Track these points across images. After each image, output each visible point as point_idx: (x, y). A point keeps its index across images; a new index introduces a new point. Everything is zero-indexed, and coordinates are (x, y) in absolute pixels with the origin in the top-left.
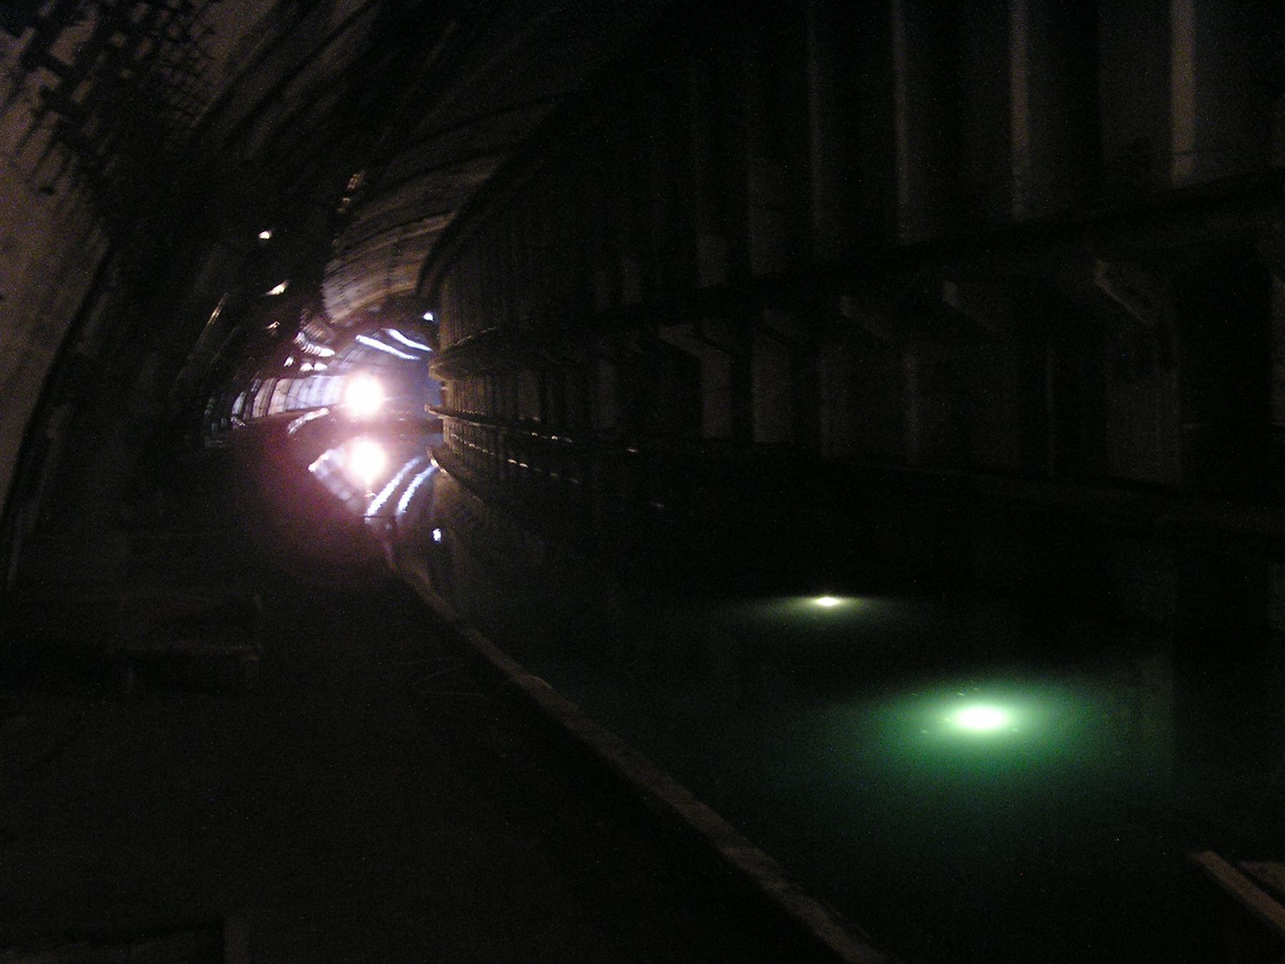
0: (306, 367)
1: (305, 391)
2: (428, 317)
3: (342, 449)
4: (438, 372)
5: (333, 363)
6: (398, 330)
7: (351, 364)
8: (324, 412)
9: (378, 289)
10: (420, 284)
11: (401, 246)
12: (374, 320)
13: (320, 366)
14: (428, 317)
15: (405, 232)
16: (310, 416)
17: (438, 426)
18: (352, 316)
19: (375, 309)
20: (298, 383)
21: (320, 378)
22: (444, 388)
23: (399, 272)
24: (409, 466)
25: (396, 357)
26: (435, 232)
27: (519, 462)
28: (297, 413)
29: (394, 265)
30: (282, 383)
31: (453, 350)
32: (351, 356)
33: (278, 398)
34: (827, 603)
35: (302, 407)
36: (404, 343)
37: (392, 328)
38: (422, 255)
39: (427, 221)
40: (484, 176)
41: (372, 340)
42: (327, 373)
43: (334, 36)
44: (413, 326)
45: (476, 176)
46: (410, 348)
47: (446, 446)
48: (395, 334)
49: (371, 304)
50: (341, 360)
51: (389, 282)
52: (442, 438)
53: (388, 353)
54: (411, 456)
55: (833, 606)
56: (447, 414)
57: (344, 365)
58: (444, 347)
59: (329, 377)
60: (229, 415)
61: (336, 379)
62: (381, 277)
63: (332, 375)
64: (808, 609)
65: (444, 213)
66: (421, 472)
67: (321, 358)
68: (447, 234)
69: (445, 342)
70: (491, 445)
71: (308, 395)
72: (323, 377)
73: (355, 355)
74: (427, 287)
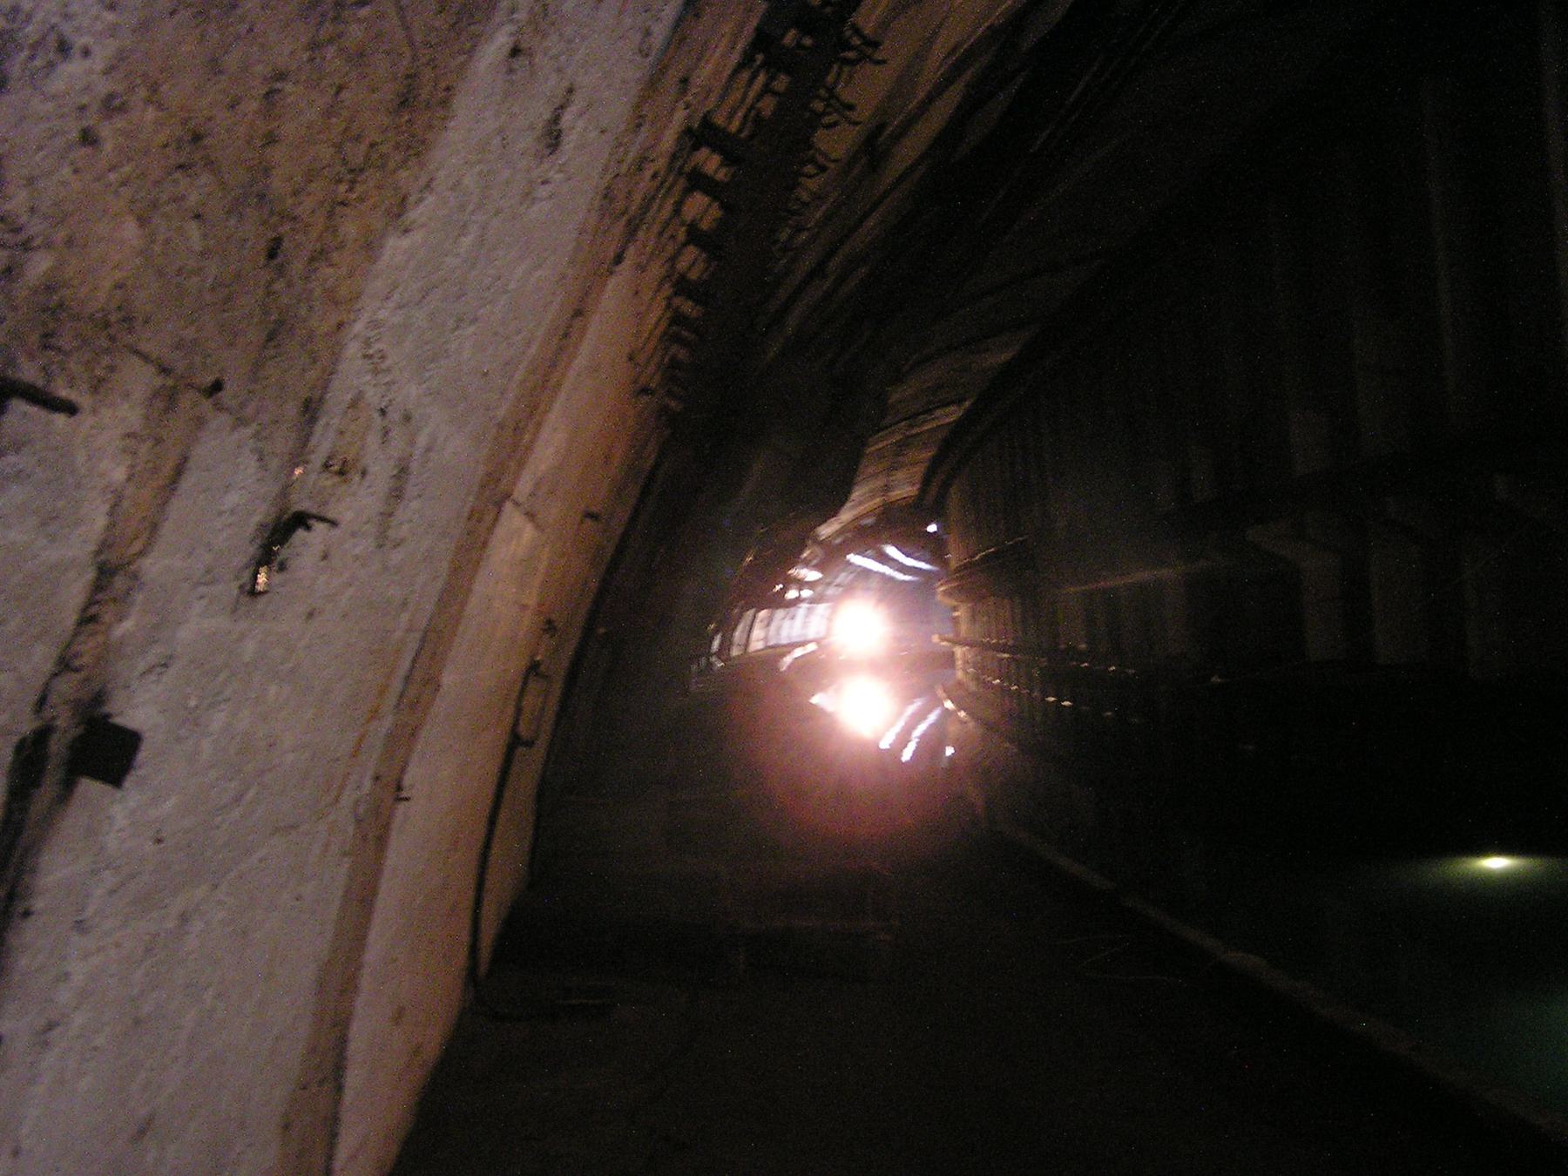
0: (792, 594)
1: (787, 623)
2: (932, 528)
3: (831, 691)
4: (947, 593)
5: (819, 589)
6: (893, 545)
7: (841, 589)
8: (811, 647)
9: (872, 497)
10: (923, 491)
11: (903, 445)
12: (866, 536)
13: (806, 593)
14: (932, 528)
15: (911, 426)
16: (798, 652)
17: (949, 659)
18: (839, 533)
19: (869, 521)
20: (780, 613)
21: (804, 606)
22: (956, 614)
23: (900, 475)
24: (911, 709)
25: (891, 579)
26: (949, 424)
27: (1060, 700)
28: (785, 649)
29: (893, 468)
30: (763, 614)
31: (967, 569)
32: (838, 581)
33: (757, 633)
34: (1496, 863)
35: (784, 642)
36: (901, 561)
37: (887, 543)
38: (928, 454)
39: (938, 413)
40: (1004, 357)
41: (866, 559)
42: (813, 601)
43: (880, 201)
44: (912, 540)
45: (999, 356)
46: (907, 567)
47: (960, 684)
48: (891, 551)
49: (862, 516)
50: (829, 584)
51: (887, 488)
52: (954, 674)
53: (883, 575)
54: (908, 700)
55: (1498, 869)
56: (967, 645)
57: (831, 591)
58: (954, 564)
59: (814, 605)
60: (709, 655)
61: (821, 608)
62: (879, 483)
63: (818, 603)
64: (1473, 873)
65: (960, 401)
66: (36, 784)
67: (808, 583)
68: (959, 429)
69: (954, 558)
70: (1023, 681)
71: (791, 627)
72: (807, 605)
73: (843, 577)
74: (934, 490)
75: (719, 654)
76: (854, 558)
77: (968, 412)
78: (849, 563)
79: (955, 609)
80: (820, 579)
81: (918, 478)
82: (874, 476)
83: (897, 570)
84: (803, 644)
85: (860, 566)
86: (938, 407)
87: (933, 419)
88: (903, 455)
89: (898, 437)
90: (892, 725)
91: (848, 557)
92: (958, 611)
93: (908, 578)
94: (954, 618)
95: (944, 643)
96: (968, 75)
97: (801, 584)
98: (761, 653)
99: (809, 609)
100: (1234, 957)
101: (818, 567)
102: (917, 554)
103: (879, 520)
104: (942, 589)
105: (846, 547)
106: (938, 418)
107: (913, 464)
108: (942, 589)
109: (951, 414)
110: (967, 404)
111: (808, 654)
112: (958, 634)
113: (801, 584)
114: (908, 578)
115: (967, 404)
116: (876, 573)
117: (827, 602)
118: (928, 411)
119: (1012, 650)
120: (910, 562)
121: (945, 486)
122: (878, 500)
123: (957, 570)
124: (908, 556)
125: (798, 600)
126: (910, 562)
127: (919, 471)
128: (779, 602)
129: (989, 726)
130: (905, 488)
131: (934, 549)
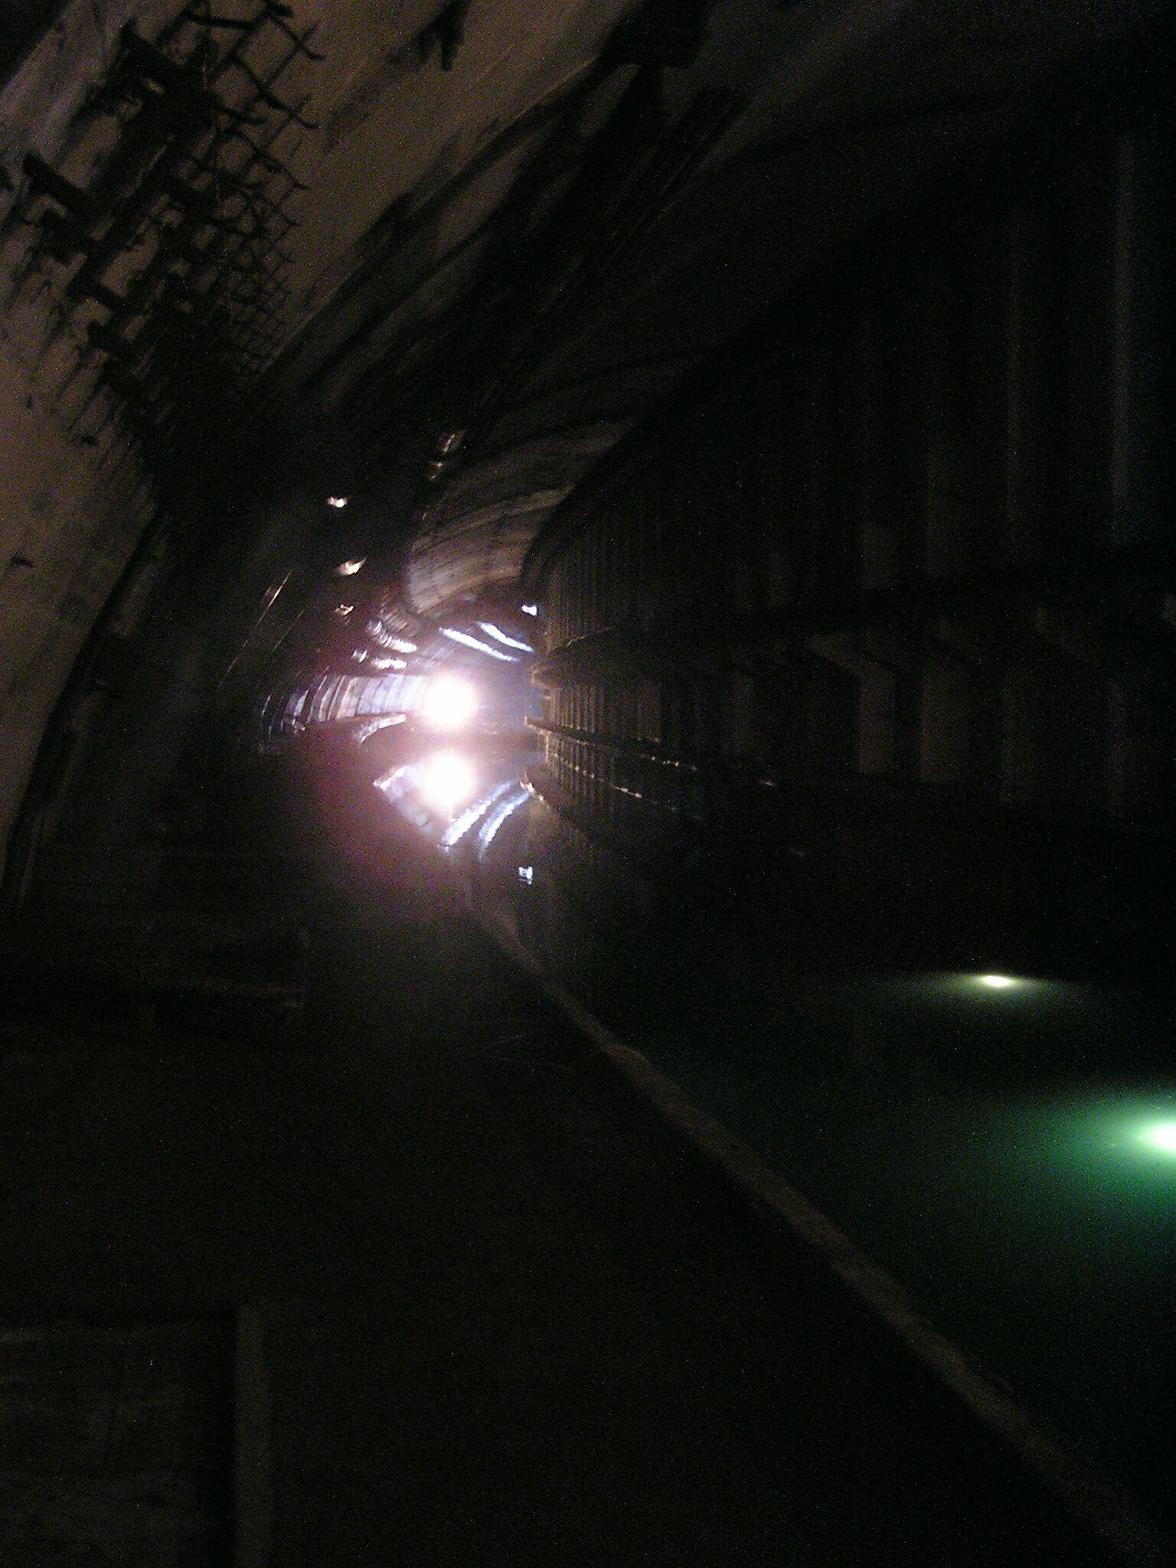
1: (381, 692)
8: (401, 719)
12: (462, 612)
13: (399, 664)
16: (384, 723)
20: (373, 682)
23: (501, 554)
30: (354, 681)
33: (346, 699)
34: (996, 982)
38: (529, 536)
45: (597, 443)
47: (544, 768)
48: (490, 629)
57: (428, 665)
58: (550, 646)
61: (417, 681)
76: (449, 633)
77: (569, 498)
78: (448, 639)
84: (385, 715)
85: (458, 643)
92: (548, 695)
93: (509, 658)
95: (531, 726)
96: (517, 153)
97: (395, 654)
101: (414, 640)
102: (520, 636)
103: (480, 597)
107: (515, 543)
110: (568, 490)
111: (395, 726)
112: (546, 718)
113: (395, 654)
114: (509, 658)
119: (582, 735)
122: (479, 579)
124: (508, 636)
127: (519, 552)
128: (366, 671)
129: (566, 814)
131: (529, 629)
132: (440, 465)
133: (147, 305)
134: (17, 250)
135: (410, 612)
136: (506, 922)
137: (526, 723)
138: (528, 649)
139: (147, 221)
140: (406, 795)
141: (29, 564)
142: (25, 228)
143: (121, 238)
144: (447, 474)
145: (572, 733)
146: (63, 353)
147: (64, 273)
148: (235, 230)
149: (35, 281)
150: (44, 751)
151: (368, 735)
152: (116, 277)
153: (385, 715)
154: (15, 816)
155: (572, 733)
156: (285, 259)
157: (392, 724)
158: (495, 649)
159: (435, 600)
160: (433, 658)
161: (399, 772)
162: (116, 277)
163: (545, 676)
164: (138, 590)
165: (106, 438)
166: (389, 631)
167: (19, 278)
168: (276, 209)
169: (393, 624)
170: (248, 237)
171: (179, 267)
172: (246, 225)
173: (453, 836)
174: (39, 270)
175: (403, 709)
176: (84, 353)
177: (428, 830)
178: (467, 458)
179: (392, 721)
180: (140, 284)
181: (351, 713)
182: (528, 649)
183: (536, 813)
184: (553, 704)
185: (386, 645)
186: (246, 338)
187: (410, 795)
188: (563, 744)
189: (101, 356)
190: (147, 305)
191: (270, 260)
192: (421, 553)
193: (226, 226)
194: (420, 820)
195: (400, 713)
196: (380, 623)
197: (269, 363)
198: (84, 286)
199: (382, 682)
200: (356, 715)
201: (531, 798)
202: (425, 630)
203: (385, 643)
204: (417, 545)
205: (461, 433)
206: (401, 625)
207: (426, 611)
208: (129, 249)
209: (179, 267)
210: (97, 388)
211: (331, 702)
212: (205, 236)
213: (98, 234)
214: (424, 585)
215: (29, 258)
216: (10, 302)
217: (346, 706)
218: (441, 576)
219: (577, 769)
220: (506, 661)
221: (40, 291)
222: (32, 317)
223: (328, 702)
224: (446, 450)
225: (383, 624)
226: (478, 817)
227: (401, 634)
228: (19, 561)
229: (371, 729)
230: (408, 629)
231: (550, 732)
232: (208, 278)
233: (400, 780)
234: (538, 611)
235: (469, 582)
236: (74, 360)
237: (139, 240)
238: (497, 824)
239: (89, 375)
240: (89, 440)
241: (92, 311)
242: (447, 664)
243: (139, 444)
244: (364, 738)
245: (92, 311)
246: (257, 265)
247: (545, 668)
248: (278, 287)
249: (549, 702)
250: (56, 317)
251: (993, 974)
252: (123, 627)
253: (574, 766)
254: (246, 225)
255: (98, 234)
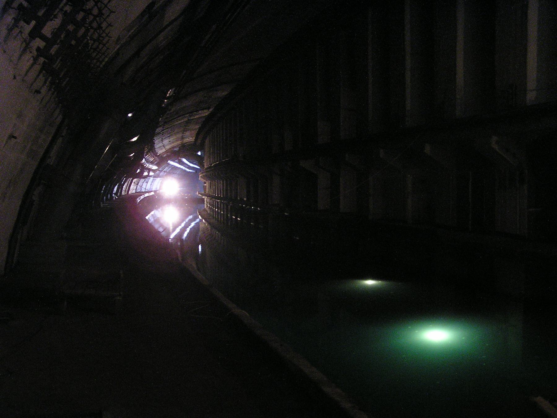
6: (184, 158)
8: (152, 193)
9: (177, 140)
10: (196, 139)
11: (188, 122)
12: (175, 154)
14: (199, 153)
15: (190, 116)
16: (146, 195)
20: (142, 180)
21: (152, 179)
22: (205, 185)
23: (188, 133)
25: (185, 171)
28: (141, 194)
29: (185, 130)
33: (133, 187)
34: (370, 283)
38: (197, 127)
39: (200, 112)
42: (154, 177)
44: (193, 157)
45: (222, 93)
47: (205, 210)
48: (184, 160)
49: (173, 147)
51: (182, 138)
53: (182, 169)
58: (206, 167)
61: (158, 180)
62: (180, 135)
65: (209, 108)
68: (208, 119)
75: (116, 194)
77: (211, 113)
78: (169, 164)
79: (205, 183)
80: (157, 169)
81: (194, 135)
82: (178, 133)
83: (187, 168)
84: (146, 192)
86: (200, 110)
87: (198, 114)
88: (189, 126)
89: (186, 119)
90: (183, 222)
91: (169, 161)
93: (191, 171)
94: (204, 186)
95: (199, 195)
97: (149, 170)
98: (134, 194)
99: (153, 179)
100: (237, 311)
101: (156, 165)
103: (180, 149)
104: (201, 175)
105: (169, 157)
106: (200, 114)
108: (201, 175)
109: (206, 113)
110: (211, 110)
114: (191, 171)
115: (211, 110)
116: (179, 168)
117: (160, 178)
118: (197, 111)
120: (191, 165)
121: (204, 138)
122: (179, 142)
123: (206, 169)
124: (190, 162)
125: (148, 176)
126: (191, 165)
127: (194, 133)
128: (140, 176)
130: (189, 138)
131: (200, 161)
132: (166, 101)
133: (59, 41)
134: (9, 19)
135: (155, 154)
136: (192, 264)
137: (197, 194)
138: (198, 167)
139: (58, 10)
140: (155, 221)
141: (15, 138)
142: (11, 10)
143: (48, 17)
144: (170, 104)
145: (218, 198)
146: (28, 59)
147: (28, 28)
148: (91, 14)
149: (17, 30)
150: (21, 207)
151: (141, 199)
152: (47, 31)
153: (146, 192)
154: (458, 29)
155: (218, 198)
156: (110, 25)
157: (149, 195)
158: (186, 167)
159: (164, 150)
160: (163, 171)
161: (152, 213)
162: (47, 31)
163: (205, 177)
164: (55, 148)
165: (44, 91)
166: (147, 161)
167: (10, 30)
168: (106, 6)
169: (150, 159)
170: (95, 17)
171: (71, 27)
172: (95, 11)
173: (172, 236)
174: (17, 27)
175: (153, 190)
176: (35, 59)
177: (163, 234)
178: (175, 99)
179: (149, 194)
180: (56, 34)
181: (134, 191)
182: (198, 167)
183: (202, 226)
184: (207, 188)
185: (146, 167)
186: (95, 54)
187: (157, 220)
188: (211, 201)
189: (42, 60)
190: (59, 41)
191: (104, 25)
192: (159, 134)
193: (88, 12)
194: (161, 230)
195: (152, 191)
196: (144, 159)
197: (104, 63)
198: (35, 33)
199: (145, 180)
200: (136, 192)
201: (201, 221)
202: (161, 161)
203: (146, 166)
204: (158, 130)
205: (174, 89)
206: (152, 159)
207: (161, 154)
208: (51, 20)
209: (71, 27)
210: (40, 72)
211: (126, 188)
212: (80, 16)
213: (40, 13)
214: (161, 145)
215: (13, 22)
216: (6, 40)
217: (133, 190)
218: (166, 142)
219: (214, 209)
220: (190, 171)
221: (17, 35)
222: (16, 45)
223: (126, 188)
224: (168, 95)
225: (145, 159)
226: (189, 229)
227: (152, 163)
228: (12, 137)
229: (142, 197)
230: (154, 161)
231: (206, 197)
232: (82, 31)
233: (152, 215)
234: (198, 155)
235: (175, 144)
236: (31, 61)
237: (55, 17)
238: (188, 230)
239: (37, 67)
240: (38, 92)
241: (38, 43)
242: (169, 173)
243: (56, 93)
244: (139, 200)
245: (38, 43)
246: (100, 27)
247: (204, 174)
248: (107, 35)
249: (206, 186)
250: (24, 44)
251: (369, 280)
252: (52, 160)
253: (213, 208)
254: (95, 11)
255: (40, 13)
